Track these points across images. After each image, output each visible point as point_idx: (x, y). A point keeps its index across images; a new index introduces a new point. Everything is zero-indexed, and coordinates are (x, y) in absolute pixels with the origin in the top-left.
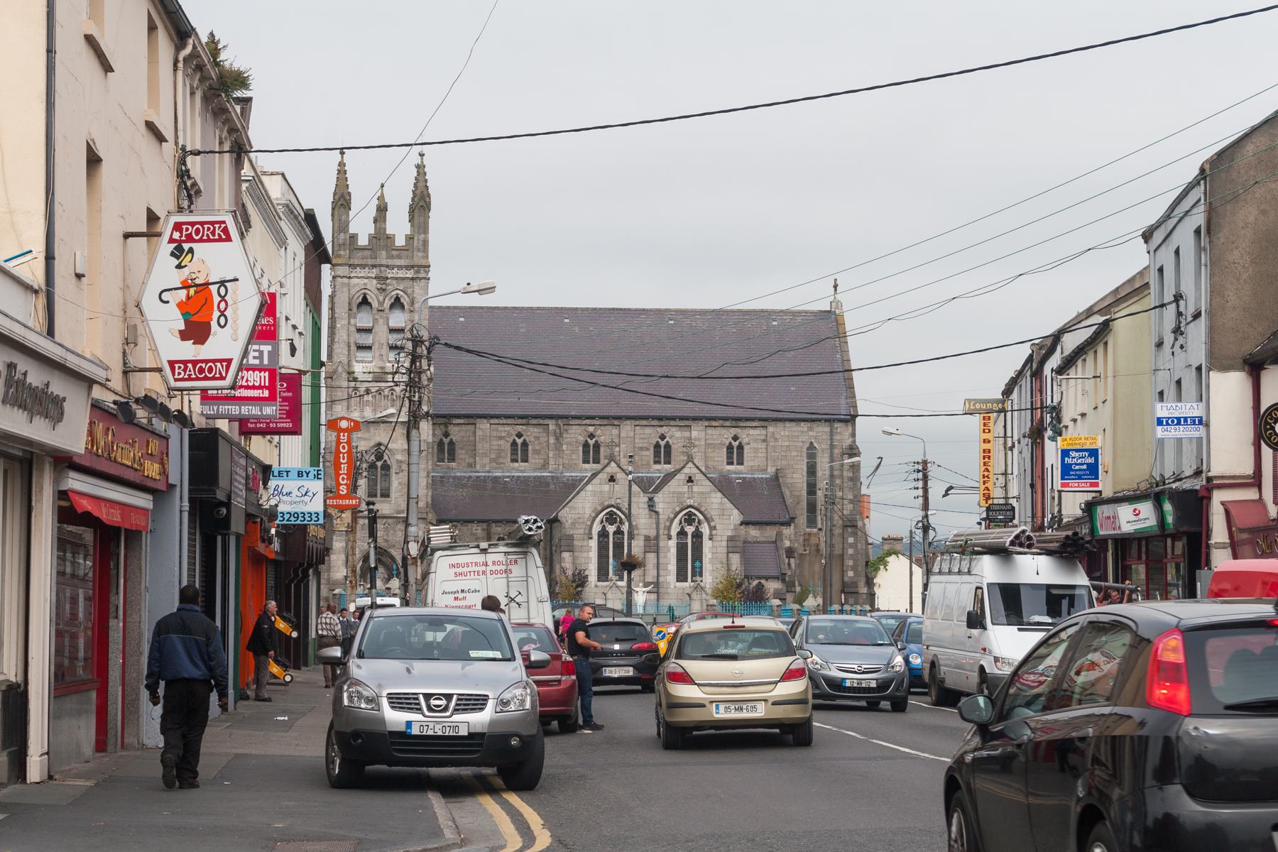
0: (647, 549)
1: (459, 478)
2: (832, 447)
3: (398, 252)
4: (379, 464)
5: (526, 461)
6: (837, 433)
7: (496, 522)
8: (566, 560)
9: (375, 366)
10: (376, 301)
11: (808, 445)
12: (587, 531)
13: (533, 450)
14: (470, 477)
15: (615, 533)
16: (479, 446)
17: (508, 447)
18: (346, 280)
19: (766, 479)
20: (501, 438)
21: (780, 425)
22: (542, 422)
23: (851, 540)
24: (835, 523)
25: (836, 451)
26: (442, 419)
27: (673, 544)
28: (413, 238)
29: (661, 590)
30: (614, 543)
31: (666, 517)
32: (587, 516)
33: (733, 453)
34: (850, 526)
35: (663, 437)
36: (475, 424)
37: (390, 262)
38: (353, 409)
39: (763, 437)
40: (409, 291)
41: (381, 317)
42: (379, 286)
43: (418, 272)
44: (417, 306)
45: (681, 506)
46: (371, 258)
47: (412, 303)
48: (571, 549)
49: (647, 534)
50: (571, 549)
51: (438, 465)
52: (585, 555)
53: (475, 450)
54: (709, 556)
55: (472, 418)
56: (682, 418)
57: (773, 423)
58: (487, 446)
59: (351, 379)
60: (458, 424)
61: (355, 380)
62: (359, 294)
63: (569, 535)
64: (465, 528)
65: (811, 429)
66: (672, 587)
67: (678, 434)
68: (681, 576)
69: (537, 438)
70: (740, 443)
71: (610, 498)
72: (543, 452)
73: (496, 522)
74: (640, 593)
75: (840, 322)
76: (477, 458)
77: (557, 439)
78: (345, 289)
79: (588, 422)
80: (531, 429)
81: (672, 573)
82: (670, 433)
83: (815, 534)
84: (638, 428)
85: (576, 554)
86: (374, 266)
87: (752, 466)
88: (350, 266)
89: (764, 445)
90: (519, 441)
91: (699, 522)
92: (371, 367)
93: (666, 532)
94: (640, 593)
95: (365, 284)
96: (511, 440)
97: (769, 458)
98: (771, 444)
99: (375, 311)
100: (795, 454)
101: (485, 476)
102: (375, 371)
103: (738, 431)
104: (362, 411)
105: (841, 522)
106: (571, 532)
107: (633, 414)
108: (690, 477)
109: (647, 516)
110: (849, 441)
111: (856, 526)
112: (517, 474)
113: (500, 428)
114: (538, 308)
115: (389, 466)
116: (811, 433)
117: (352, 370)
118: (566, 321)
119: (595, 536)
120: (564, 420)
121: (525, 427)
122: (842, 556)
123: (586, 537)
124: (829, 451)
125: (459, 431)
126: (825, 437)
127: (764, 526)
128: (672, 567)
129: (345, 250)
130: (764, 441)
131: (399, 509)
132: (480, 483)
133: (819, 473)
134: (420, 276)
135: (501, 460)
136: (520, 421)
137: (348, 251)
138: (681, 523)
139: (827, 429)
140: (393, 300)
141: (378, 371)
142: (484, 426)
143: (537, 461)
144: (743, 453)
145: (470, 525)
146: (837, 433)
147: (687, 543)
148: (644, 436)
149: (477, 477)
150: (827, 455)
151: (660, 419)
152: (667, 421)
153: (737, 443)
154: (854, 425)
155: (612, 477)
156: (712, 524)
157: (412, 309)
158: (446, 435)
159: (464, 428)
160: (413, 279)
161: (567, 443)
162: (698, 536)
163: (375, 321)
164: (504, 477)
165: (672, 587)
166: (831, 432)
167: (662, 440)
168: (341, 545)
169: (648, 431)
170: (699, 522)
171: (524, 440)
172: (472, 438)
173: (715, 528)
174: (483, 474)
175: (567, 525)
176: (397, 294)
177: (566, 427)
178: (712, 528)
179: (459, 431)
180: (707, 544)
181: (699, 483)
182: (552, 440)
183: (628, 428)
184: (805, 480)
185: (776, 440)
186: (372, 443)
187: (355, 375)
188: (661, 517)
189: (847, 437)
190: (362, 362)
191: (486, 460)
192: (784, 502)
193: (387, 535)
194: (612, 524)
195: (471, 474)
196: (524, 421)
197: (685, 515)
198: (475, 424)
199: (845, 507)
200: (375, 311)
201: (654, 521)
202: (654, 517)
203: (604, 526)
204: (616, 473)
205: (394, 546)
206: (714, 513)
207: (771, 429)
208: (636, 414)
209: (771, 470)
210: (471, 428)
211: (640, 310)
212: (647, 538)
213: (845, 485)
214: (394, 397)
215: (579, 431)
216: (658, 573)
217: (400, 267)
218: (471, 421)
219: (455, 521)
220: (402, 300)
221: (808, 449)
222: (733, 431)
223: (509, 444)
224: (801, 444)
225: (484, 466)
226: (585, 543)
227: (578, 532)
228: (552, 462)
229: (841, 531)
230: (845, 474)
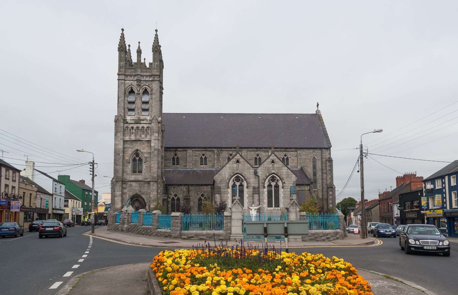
0: (254, 193)
1: (180, 171)
2: (322, 158)
3: (146, 70)
4: (137, 158)
5: (206, 165)
6: (324, 153)
7: (191, 185)
8: (217, 198)
9: (136, 117)
10: (136, 90)
11: (313, 158)
12: (227, 185)
13: (209, 160)
14: (184, 170)
15: (239, 186)
16: (188, 159)
17: (199, 159)
18: (123, 81)
19: (297, 170)
20: (196, 156)
21: (302, 150)
22: (212, 150)
23: (331, 193)
24: (324, 187)
25: (324, 160)
26: (174, 149)
27: (266, 190)
28: (152, 64)
29: (261, 211)
30: (239, 190)
31: (263, 178)
32: (227, 178)
33: (285, 161)
34: (330, 188)
35: (258, 155)
36: (186, 151)
37: (142, 74)
38: (126, 135)
39: (296, 155)
40: (151, 86)
41: (139, 97)
42: (137, 84)
43: (154, 78)
44: (154, 92)
45: (269, 173)
46: (134, 72)
47: (152, 91)
48: (220, 193)
49: (254, 186)
50: (220, 193)
51: (172, 166)
52: (226, 195)
53: (187, 160)
54: (282, 195)
55: (185, 148)
56: (265, 148)
57: (300, 149)
58: (191, 159)
59: (125, 122)
60: (180, 151)
61: (127, 123)
62: (129, 87)
63: (219, 187)
64: (179, 188)
65: (314, 152)
66: (266, 209)
67: (264, 154)
68: (270, 205)
69: (210, 156)
70: (287, 157)
71: (237, 170)
72: (212, 161)
73: (191, 185)
74: (253, 210)
75: (320, 116)
76: (187, 164)
77: (218, 156)
78: (123, 85)
79: (229, 149)
80: (208, 152)
81: (266, 203)
82: (261, 154)
83: (316, 191)
84: (248, 152)
85: (222, 195)
86: (135, 75)
87: (292, 166)
88: (125, 75)
89: (296, 158)
90: (203, 157)
91: (278, 180)
92: (134, 118)
93: (263, 185)
94: (253, 210)
95: (131, 83)
96: (200, 157)
97: (298, 162)
98: (299, 157)
99: (136, 94)
100: (308, 161)
101: (190, 170)
102: (136, 119)
103: (286, 153)
104: (130, 136)
105: (326, 186)
106: (220, 185)
107: (247, 147)
108: (273, 161)
109: (254, 178)
110: (328, 156)
111: (332, 188)
112: (202, 169)
113: (196, 152)
114: (212, 114)
115: (142, 159)
116: (314, 153)
117: (125, 119)
118: (222, 117)
119: (231, 187)
120: (221, 149)
121: (205, 152)
122: (327, 200)
123: (226, 187)
124: (321, 160)
125: (181, 154)
126: (319, 155)
127: (300, 186)
128: (266, 201)
129: (123, 69)
130: (296, 156)
131: (146, 177)
132: (188, 172)
133: (317, 168)
134: (155, 79)
135: (197, 164)
136: (204, 149)
137: (124, 69)
138: (269, 181)
139: (320, 152)
140: (144, 90)
141: (137, 119)
142: (190, 151)
143: (210, 164)
144: (288, 161)
145: (181, 187)
146: (324, 153)
147: (272, 190)
148: (251, 155)
149: (187, 170)
150: (320, 161)
151: (257, 148)
152: (260, 149)
153: (286, 157)
154: (330, 150)
155: (238, 161)
156: (283, 181)
157: (151, 93)
158: (176, 155)
159: (182, 152)
160: (152, 81)
161: (222, 158)
162: (277, 187)
163: (136, 98)
164: (197, 170)
165: (266, 209)
166: (321, 153)
167: (258, 156)
168: (119, 193)
169: (252, 153)
170: (278, 180)
171: (205, 157)
172: (185, 156)
173: (284, 183)
174: (189, 169)
175: (218, 182)
176: (146, 87)
177: (221, 152)
178: (283, 183)
179: (181, 154)
180: (281, 191)
181: (277, 163)
182: (216, 156)
183: (245, 152)
184: (312, 170)
185: (301, 156)
186: (134, 150)
187: (127, 121)
188: (260, 178)
189: (327, 155)
190: (130, 115)
191: (191, 164)
192: (306, 176)
193: (141, 189)
194: (238, 182)
195: (185, 169)
196: (205, 149)
197: (271, 177)
198: (186, 151)
199: (328, 181)
200: (136, 94)
201: (257, 180)
202: (257, 178)
203: (234, 182)
204: (239, 159)
205: (144, 194)
206: (284, 176)
207: (299, 152)
208: (248, 147)
209: (299, 167)
210: (185, 152)
211: (248, 114)
212: (254, 188)
213: (328, 172)
214: (144, 130)
215: (226, 153)
216: (259, 198)
217: (147, 76)
218: (185, 149)
219: (174, 185)
220: (148, 90)
221: (313, 159)
222: (284, 153)
223: (200, 158)
224: (310, 157)
225: (190, 166)
226: (226, 190)
227: (223, 185)
228: (216, 165)
229: (326, 190)
230: (327, 168)
